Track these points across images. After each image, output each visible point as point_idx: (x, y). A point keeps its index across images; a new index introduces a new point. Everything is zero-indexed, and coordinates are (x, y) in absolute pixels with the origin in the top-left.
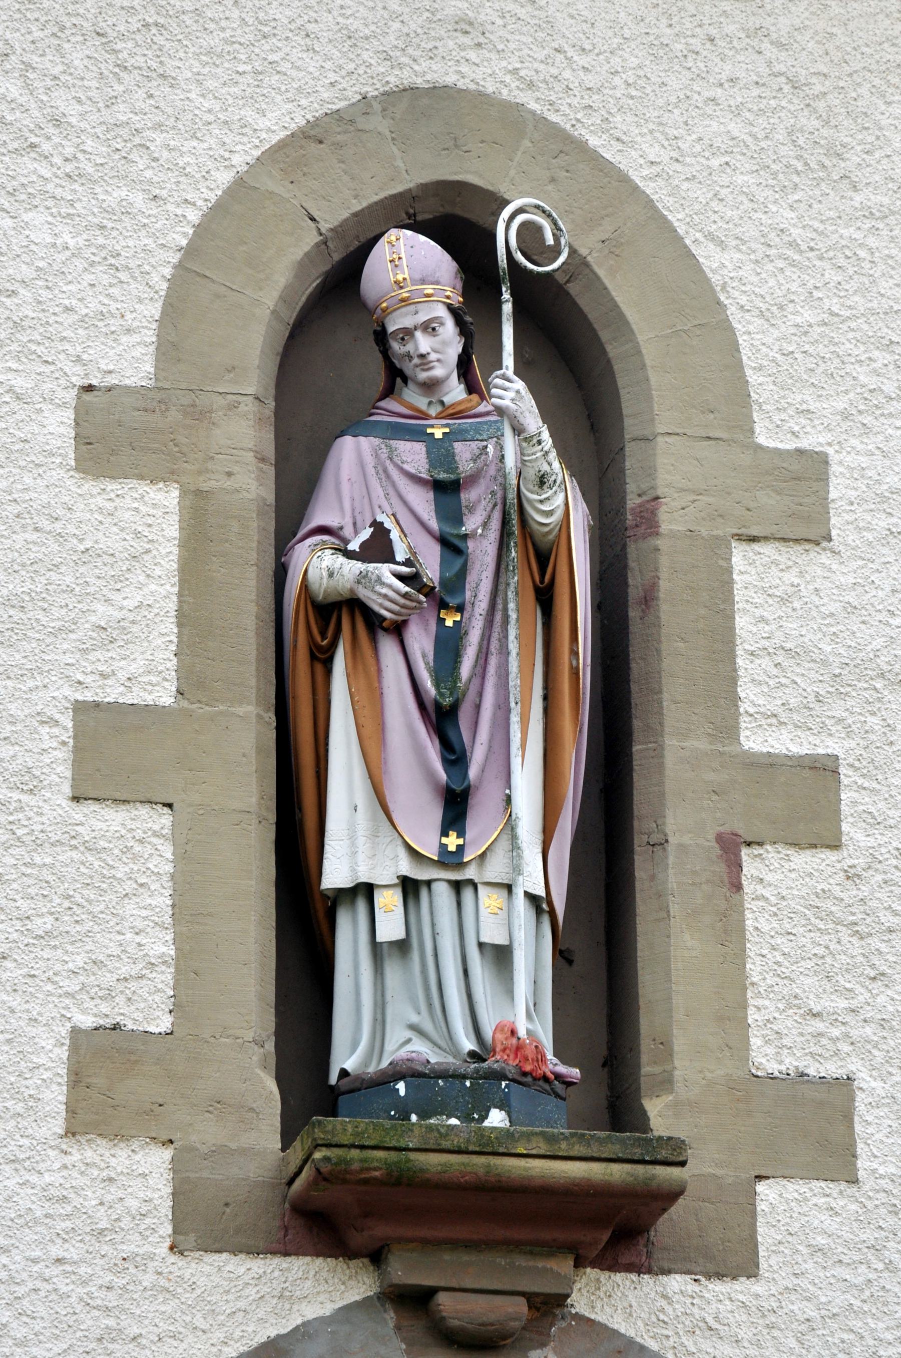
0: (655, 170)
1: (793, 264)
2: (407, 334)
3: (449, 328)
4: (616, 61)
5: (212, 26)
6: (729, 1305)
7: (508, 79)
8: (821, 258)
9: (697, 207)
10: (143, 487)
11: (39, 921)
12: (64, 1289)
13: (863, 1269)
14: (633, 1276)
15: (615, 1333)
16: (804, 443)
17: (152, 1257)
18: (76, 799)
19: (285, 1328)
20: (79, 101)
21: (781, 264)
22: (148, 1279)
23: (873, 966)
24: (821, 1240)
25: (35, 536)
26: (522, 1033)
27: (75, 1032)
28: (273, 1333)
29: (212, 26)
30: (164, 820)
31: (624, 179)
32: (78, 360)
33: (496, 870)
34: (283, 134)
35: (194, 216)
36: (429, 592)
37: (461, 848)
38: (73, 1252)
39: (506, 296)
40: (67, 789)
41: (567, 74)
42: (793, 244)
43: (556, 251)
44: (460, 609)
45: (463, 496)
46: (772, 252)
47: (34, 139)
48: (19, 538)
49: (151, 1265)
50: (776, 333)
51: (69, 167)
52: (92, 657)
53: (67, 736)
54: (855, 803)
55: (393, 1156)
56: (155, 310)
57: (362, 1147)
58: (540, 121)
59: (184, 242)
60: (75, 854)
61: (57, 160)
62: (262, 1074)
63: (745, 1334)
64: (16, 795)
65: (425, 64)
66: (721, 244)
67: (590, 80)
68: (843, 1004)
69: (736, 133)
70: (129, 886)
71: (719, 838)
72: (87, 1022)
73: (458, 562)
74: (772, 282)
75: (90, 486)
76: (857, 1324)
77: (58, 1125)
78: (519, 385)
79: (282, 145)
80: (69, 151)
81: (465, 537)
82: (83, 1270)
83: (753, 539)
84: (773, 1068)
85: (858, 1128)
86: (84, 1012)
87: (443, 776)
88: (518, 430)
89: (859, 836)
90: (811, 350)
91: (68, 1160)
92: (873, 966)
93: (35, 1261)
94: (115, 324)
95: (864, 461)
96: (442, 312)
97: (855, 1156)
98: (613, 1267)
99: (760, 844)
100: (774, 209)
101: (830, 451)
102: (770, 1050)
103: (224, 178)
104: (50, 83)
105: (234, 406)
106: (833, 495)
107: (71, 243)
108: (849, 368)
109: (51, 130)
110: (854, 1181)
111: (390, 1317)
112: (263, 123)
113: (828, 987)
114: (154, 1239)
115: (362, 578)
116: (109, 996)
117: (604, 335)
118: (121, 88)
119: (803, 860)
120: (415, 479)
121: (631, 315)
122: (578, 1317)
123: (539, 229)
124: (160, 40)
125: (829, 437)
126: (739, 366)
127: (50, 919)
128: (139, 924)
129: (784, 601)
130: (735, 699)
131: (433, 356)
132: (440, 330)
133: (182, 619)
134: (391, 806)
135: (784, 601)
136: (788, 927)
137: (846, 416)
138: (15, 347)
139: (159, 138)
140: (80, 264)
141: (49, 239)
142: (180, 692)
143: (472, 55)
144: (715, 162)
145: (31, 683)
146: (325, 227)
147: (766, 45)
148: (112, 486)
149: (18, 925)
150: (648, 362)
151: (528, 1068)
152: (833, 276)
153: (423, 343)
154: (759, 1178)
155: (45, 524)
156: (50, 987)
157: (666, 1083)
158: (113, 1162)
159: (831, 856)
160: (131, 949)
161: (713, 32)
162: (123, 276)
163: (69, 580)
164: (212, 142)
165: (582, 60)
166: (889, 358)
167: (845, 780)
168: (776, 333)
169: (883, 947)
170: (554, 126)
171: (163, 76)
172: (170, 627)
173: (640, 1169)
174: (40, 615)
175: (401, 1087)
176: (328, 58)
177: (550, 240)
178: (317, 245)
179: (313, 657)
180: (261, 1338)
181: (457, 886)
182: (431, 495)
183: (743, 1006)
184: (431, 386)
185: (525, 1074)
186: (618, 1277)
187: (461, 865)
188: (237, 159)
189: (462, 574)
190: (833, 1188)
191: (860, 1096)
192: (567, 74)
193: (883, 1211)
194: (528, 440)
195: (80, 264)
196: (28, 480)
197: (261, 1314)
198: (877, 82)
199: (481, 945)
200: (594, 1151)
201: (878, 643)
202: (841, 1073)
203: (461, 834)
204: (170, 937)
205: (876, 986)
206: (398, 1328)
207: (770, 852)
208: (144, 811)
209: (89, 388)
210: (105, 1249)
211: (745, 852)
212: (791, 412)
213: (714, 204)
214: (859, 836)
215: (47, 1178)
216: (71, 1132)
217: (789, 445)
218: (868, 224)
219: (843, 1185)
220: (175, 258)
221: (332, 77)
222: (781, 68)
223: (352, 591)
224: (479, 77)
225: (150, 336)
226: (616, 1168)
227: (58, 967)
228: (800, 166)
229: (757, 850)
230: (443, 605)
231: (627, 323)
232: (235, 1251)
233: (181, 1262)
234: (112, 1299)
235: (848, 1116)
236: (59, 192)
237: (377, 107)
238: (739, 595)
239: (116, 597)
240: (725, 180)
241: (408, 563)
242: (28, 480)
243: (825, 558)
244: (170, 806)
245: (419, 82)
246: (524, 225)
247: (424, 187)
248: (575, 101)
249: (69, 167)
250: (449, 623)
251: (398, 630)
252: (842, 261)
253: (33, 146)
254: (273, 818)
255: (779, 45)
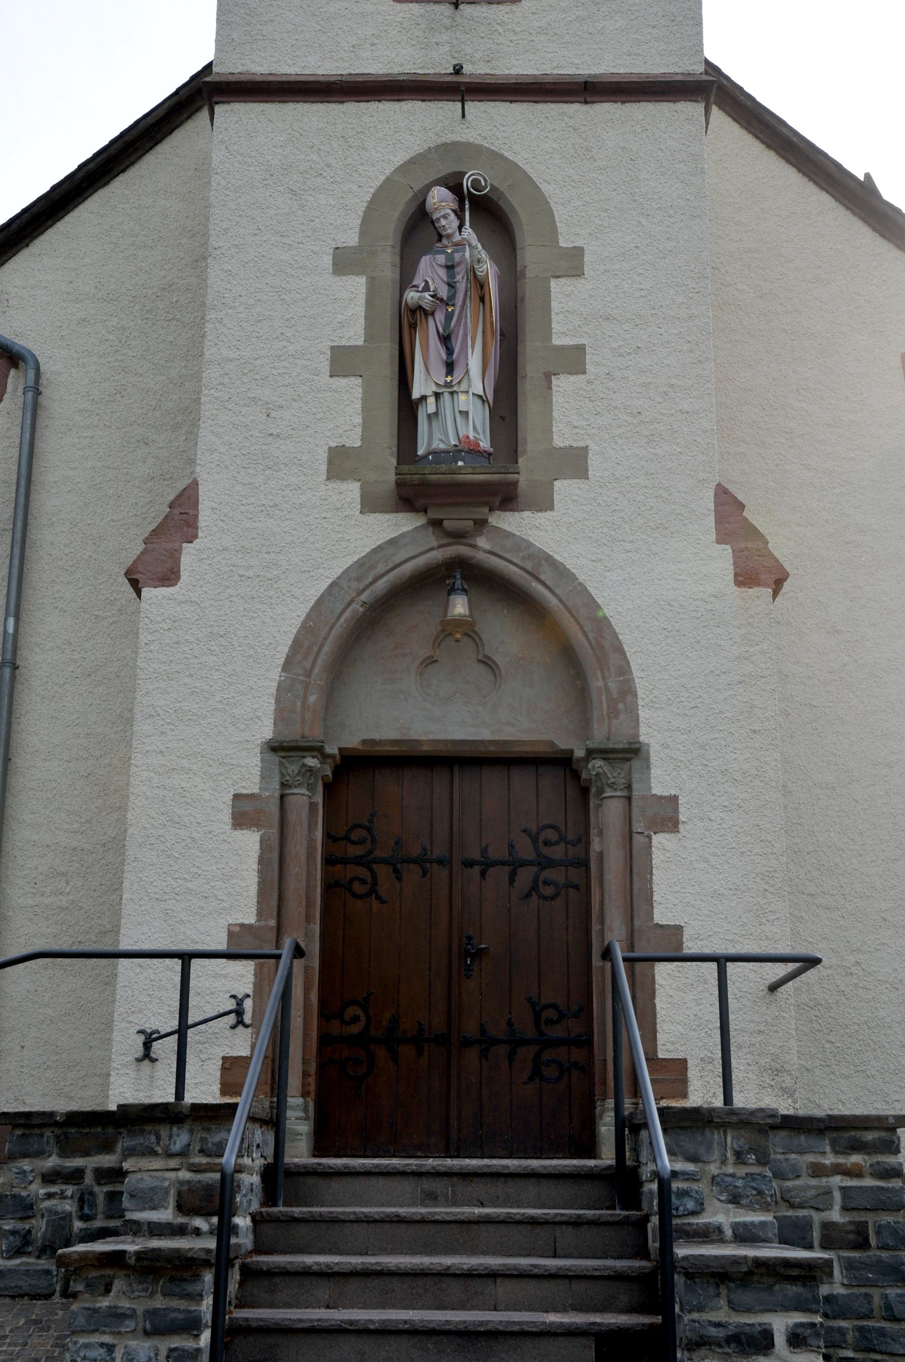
0: (527, 161)
1: (573, 187)
2: (438, 219)
3: (452, 216)
4: (514, 128)
5: (379, 131)
6: (544, 520)
7: (478, 137)
8: (583, 184)
9: (541, 172)
10: (354, 277)
11: (319, 415)
12: (326, 526)
13: (590, 506)
14: (512, 513)
15: (506, 531)
16: (576, 245)
17: (354, 515)
18: (331, 376)
19: (396, 534)
20: (336, 159)
21: (569, 187)
22: (353, 522)
23: (596, 410)
24: (575, 498)
25: (319, 296)
26: (471, 437)
27: (330, 448)
28: (392, 536)
29: (379, 131)
30: (359, 381)
31: (516, 165)
32: (334, 239)
33: (463, 387)
34: (402, 162)
35: (372, 191)
36: (441, 300)
37: (451, 381)
38: (329, 515)
39: (467, 202)
40: (328, 374)
41: (498, 133)
42: (573, 181)
43: (486, 187)
44: (453, 305)
45: (456, 269)
46: (566, 184)
47: (321, 172)
48: (314, 297)
49: (354, 518)
50: (567, 210)
51: (332, 180)
52: (337, 332)
53: (328, 357)
54: (591, 359)
55: (421, 476)
56: (359, 221)
57: (411, 474)
58: (488, 149)
59: (369, 199)
60: (331, 394)
61: (328, 178)
62: (390, 457)
63: (549, 528)
64: (312, 377)
65: (450, 135)
66: (549, 183)
67: (505, 135)
68: (586, 423)
69: (554, 147)
70: (348, 402)
71: (544, 373)
72: (333, 445)
73: (453, 291)
74: (566, 194)
75: (337, 279)
76: (587, 523)
77: (325, 477)
78: (470, 230)
79: (401, 166)
80: (332, 175)
81: (456, 282)
82: (332, 520)
83: (558, 277)
84: (561, 445)
85: (589, 462)
86: (333, 442)
87: (445, 358)
88: (470, 245)
89: (593, 369)
90: (579, 214)
91: (328, 487)
92: (596, 410)
93: (317, 518)
94: (346, 227)
95: (596, 248)
96: (449, 211)
97: (588, 471)
98: (505, 510)
99: (559, 374)
100: (567, 169)
101: (585, 246)
102: (561, 440)
103: (383, 178)
104: (326, 154)
105: (384, 249)
106: (585, 260)
107: (332, 203)
108: (592, 219)
109: (326, 169)
110: (587, 478)
111: (431, 529)
112: (396, 159)
113: (581, 418)
114: (355, 510)
115: (420, 297)
116: (341, 437)
117: (510, 216)
118: (349, 153)
119: (573, 378)
120: (441, 266)
121: (518, 208)
122: (493, 526)
123: (480, 181)
124: (362, 137)
125: (585, 242)
126: (554, 222)
127: (322, 414)
128: (351, 414)
129: (568, 296)
130: (551, 328)
131: (447, 226)
132: (449, 217)
133: (366, 318)
134: (430, 370)
135: (568, 296)
136: (567, 400)
137: (590, 234)
138: (314, 237)
139: (362, 168)
140: (335, 209)
141: (325, 203)
142: (365, 341)
143: (466, 131)
144: (547, 157)
145: (317, 342)
146: (415, 190)
147: (565, 117)
148: (344, 278)
149: (312, 416)
150: (523, 223)
151: (471, 448)
152: (587, 190)
153: (443, 222)
154: (555, 480)
155: (322, 291)
156: (322, 435)
157: (525, 452)
158: (342, 487)
159: (582, 376)
160: (349, 422)
161: (547, 115)
162: (349, 212)
163: (330, 308)
164: (379, 167)
165: (503, 129)
166: (606, 214)
167: (587, 352)
168: (567, 210)
169: (600, 404)
170: (493, 151)
171: (363, 148)
172: (363, 320)
173: (503, 476)
174: (320, 320)
175: (430, 457)
176: (417, 137)
177: (483, 184)
178: (413, 196)
179: (410, 327)
180: (389, 538)
181: (452, 393)
182: (445, 270)
183: (551, 426)
184: (449, 236)
185: (471, 450)
186: (507, 513)
187: (452, 386)
188: (387, 172)
189: (454, 294)
190: (580, 481)
191: (590, 452)
192: (498, 133)
193: (597, 487)
194: (473, 248)
195: (335, 209)
196: (317, 278)
197: (389, 531)
198: (603, 126)
199: (460, 412)
200: (488, 471)
201: (600, 307)
202: (585, 445)
203: (452, 376)
204: (361, 417)
205: (597, 417)
206: (433, 533)
207: (562, 376)
208: (353, 378)
209: (338, 248)
210: (339, 514)
211: (553, 377)
212: (572, 234)
213: (547, 171)
214: (593, 369)
215: (321, 493)
216: (328, 479)
217: (571, 245)
218: (599, 171)
219: (583, 480)
220: (366, 204)
221: (419, 142)
222: (571, 124)
223: (418, 303)
224: (467, 137)
225: (357, 230)
226: (495, 476)
227: (325, 428)
228: (576, 155)
229: (557, 376)
230: (447, 304)
231: (516, 211)
232: (381, 512)
233: (363, 516)
234: (341, 529)
235: (586, 458)
236: (329, 188)
237: (434, 150)
238: (553, 295)
239: (346, 312)
240: (550, 162)
241: (434, 291)
242: (317, 278)
243: (583, 281)
244: (361, 376)
245: (448, 141)
246: (472, 181)
247: (449, 174)
248: (500, 142)
249: (332, 180)
250: (450, 310)
251: (433, 314)
252: (590, 185)
253: (321, 174)
254: (397, 378)
255: (570, 117)
